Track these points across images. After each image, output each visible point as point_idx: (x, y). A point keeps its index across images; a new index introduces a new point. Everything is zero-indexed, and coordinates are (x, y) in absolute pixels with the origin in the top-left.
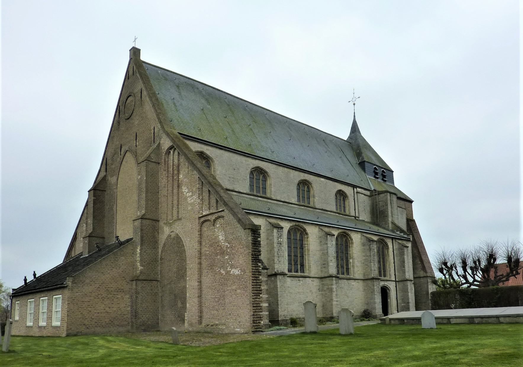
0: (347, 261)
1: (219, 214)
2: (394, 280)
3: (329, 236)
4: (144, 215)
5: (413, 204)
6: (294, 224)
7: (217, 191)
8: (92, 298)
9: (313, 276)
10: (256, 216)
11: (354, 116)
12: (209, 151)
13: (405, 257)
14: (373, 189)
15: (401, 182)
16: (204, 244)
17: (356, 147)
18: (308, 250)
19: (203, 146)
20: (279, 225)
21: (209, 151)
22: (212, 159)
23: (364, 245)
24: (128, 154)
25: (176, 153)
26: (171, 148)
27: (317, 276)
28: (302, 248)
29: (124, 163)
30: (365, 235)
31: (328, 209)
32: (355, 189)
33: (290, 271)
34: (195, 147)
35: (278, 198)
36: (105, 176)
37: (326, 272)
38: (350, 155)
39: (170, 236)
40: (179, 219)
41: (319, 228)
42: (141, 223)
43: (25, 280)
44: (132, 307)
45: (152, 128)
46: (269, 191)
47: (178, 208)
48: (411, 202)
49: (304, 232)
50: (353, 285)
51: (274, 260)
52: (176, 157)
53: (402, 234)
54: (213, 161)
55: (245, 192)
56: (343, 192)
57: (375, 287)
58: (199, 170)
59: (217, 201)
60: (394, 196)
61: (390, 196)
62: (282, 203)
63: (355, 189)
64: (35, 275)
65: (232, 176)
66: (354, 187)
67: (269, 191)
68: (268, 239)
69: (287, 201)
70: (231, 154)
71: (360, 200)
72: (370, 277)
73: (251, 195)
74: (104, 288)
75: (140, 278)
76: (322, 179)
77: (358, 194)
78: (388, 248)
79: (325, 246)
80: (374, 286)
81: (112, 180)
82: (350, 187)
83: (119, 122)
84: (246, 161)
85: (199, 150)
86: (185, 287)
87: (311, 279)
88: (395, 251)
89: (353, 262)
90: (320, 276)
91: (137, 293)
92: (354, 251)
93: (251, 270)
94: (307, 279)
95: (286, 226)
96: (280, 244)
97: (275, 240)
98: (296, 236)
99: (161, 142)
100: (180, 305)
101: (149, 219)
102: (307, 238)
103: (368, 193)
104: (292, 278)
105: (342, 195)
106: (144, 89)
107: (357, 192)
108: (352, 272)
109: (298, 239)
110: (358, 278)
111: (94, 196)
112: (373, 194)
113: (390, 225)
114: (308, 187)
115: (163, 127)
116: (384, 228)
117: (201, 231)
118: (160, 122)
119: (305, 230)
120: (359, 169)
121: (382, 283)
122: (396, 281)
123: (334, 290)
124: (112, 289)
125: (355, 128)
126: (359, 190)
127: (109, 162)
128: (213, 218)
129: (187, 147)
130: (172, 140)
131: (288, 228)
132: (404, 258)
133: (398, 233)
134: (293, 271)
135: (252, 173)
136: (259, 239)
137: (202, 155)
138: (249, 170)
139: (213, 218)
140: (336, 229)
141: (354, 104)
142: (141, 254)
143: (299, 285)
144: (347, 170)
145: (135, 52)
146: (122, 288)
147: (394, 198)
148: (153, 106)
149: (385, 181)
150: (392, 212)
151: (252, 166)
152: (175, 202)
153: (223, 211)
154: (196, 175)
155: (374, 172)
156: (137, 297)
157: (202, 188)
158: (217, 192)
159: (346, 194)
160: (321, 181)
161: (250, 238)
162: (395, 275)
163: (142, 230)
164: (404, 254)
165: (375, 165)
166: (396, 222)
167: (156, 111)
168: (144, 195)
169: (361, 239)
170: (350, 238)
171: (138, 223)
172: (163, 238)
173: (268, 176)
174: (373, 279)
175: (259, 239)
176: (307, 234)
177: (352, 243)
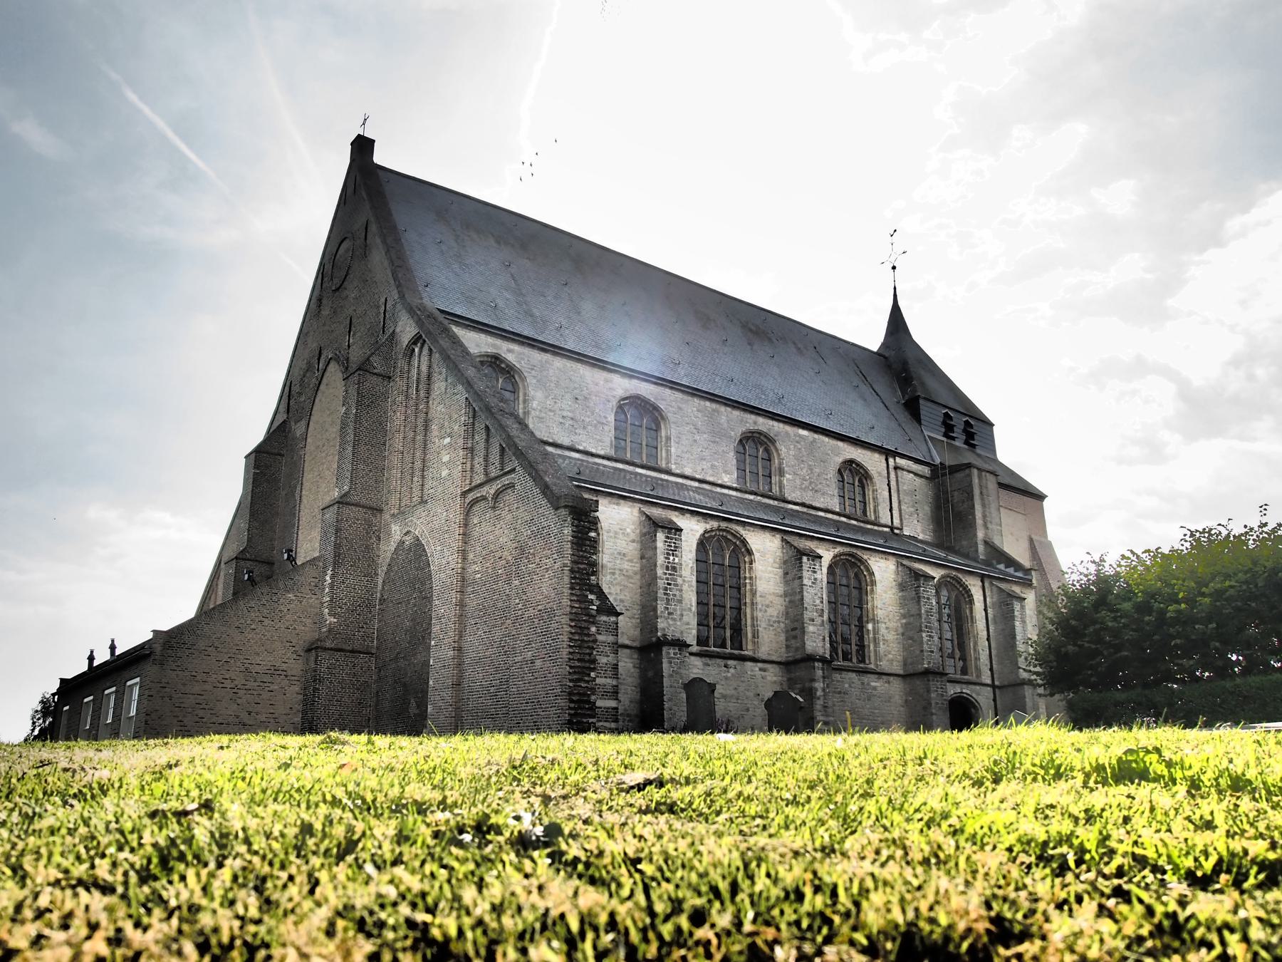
0: (861, 627)
1: (506, 480)
2: (989, 681)
3: (805, 559)
4: (345, 495)
5: (1046, 503)
6: (715, 524)
7: (501, 425)
8: (208, 687)
9: (764, 657)
10: (615, 500)
11: (895, 295)
12: (512, 353)
13: (1017, 623)
14: (938, 461)
15: (1010, 450)
16: (471, 556)
17: (901, 371)
18: (754, 593)
19: (499, 342)
20: (671, 522)
21: (512, 353)
22: (520, 372)
23: (902, 587)
24: (333, 367)
25: (425, 351)
26: (417, 340)
27: (774, 658)
28: (738, 588)
29: (322, 387)
30: (905, 562)
31: (818, 505)
32: (891, 461)
33: (701, 641)
34: (477, 343)
35: (688, 472)
36: (284, 422)
37: (797, 649)
38: (882, 385)
39: (402, 542)
40: (423, 502)
41: (783, 540)
42: (338, 513)
43: (91, 658)
44: (304, 712)
45: (383, 300)
46: (664, 454)
47: (423, 477)
48: (1040, 497)
49: (742, 550)
50: (875, 688)
51: (655, 609)
52: (425, 359)
53: (1011, 570)
54: (524, 379)
55: (602, 453)
56: (858, 464)
57: (933, 695)
58: (468, 382)
59: (502, 450)
60: (990, 477)
61: (980, 477)
62: (696, 484)
63: (891, 461)
64: (113, 648)
65: (570, 414)
66: (888, 453)
67: (664, 454)
68: (642, 557)
69: (711, 479)
70: (569, 364)
71: (904, 487)
72: (920, 668)
73: (616, 461)
74: (239, 664)
75: (328, 644)
76: (804, 433)
77: (900, 472)
78: (971, 602)
79: (797, 582)
80: (928, 691)
81: (298, 429)
82: (877, 455)
83: (320, 300)
84: (606, 381)
85: (490, 350)
86: (426, 664)
87: (760, 665)
88: (990, 611)
89: (876, 631)
90: (783, 660)
91: (317, 679)
92: (878, 603)
93: (568, 609)
94: (749, 664)
95: (692, 529)
96: (674, 569)
97: (661, 559)
98: (723, 557)
99: (398, 330)
100: (413, 710)
101: (356, 505)
102: (751, 563)
103: (926, 471)
104: (707, 660)
105: (858, 473)
106: (372, 219)
107: (896, 468)
108: (872, 654)
109: (727, 563)
110: (887, 670)
111: (256, 467)
112: (938, 475)
113: (981, 548)
114: (767, 450)
115: (402, 296)
116: (966, 556)
117: (466, 525)
118: (399, 286)
119: (744, 542)
120: (903, 416)
121: (953, 690)
122: (993, 686)
123: (819, 693)
124: (258, 669)
125: (897, 322)
126: (901, 462)
127: (296, 389)
128: (490, 490)
129: (456, 341)
130: (420, 323)
131: (698, 536)
132: (1013, 628)
133: (1001, 567)
134: (711, 642)
135: (620, 408)
136: (593, 534)
137: (495, 362)
138: (614, 403)
139: (490, 490)
140: (827, 545)
141: (894, 268)
142: (332, 586)
143: (726, 678)
144: (866, 414)
145: (362, 147)
146: (284, 666)
147: (991, 483)
148: (388, 252)
149: (974, 446)
150: (984, 516)
151: (620, 393)
152: (418, 464)
153: (513, 470)
154: (461, 394)
155: (944, 423)
156: (315, 690)
157: (473, 424)
158: (502, 428)
159: (866, 472)
160: (800, 436)
161: (568, 531)
162: (991, 669)
163: (338, 530)
164: (1013, 618)
165: (946, 407)
166: (997, 542)
167: (392, 262)
168: (350, 449)
169: (897, 573)
170: (868, 569)
171: (330, 515)
172: (387, 549)
173: (663, 418)
174: (927, 673)
175: (593, 534)
176: (750, 552)
177: (873, 583)
